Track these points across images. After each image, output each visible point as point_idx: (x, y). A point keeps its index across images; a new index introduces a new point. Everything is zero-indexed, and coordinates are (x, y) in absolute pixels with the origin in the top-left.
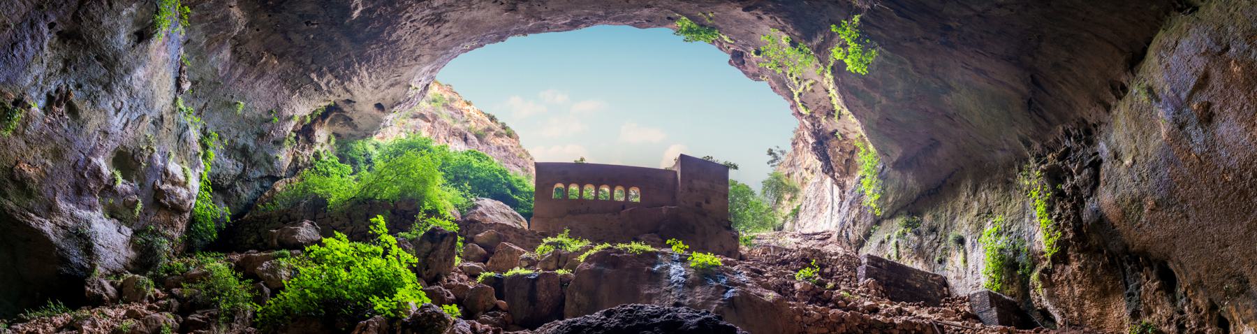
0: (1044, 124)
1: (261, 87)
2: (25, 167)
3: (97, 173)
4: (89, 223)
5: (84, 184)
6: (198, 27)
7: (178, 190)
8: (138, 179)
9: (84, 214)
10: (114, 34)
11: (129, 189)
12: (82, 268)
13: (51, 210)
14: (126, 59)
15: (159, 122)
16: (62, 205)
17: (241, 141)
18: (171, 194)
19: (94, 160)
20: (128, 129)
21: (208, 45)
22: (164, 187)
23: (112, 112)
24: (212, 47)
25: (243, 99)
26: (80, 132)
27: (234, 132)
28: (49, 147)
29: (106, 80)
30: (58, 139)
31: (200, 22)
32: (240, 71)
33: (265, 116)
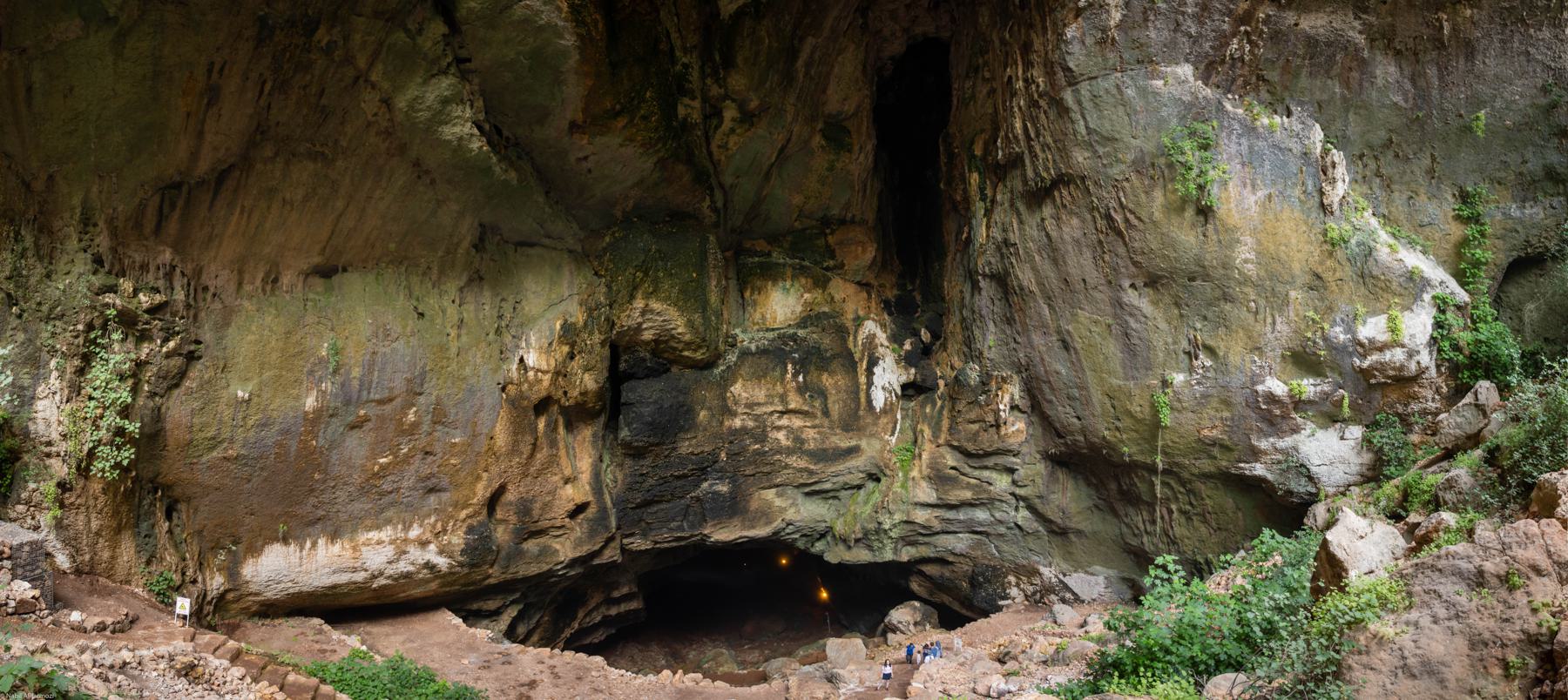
0: (149, 226)
1: (1490, 63)
2: (1206, 432)
3: (1271, 398)
4: (1296, 449)
5: (1277, 415)
6: (1304, 81)
7: (1387, 356)
8: (1332, 369)
9: (1286, 442)
10: (1173, 245)
11: (1326, 388)
12: (1311, 494)
13: (1255, 454)
14: (1212, 255)
15: (1317, 283)
16: (1263, 444)
17: (1534, 165)
18: (1381, 367)
19: (1260, 388)
20: (1278, 327)
21: (1346, 84)
22: (1366, 364)
23: (1251, 318)
24: (1354, 84)
25: (1480, 104)
26: (1229, 372)
27: (1513, 158)
28: (1215, 403)
29: (1218, 293)
30: (1214, 391)
31: (1297, 76)
32: (1432, 72)
33: (1543, 101)
